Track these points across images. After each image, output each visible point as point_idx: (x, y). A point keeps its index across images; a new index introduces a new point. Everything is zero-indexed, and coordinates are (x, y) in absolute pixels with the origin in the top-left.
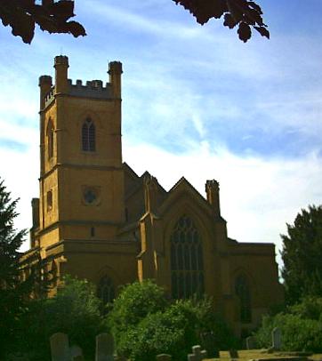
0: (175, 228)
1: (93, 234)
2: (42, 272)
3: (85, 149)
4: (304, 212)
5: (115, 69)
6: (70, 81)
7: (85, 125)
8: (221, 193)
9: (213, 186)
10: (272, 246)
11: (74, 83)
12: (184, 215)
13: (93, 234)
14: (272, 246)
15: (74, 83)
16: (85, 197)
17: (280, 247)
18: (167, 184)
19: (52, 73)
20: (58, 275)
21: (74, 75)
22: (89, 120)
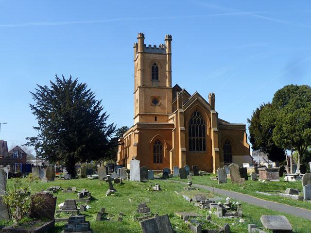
0: (192, 116)
1: (156, 120)
2: (49, 120)
3: (153, 78)
4: (258, 109)
5: (169, 39)
6: (145, 45)
7: (153, 67)
8: (216, 99)
9: (213, 97)
10: (244, 126)
11: (147, 46)
12: (197, 110)
13: (156, 120)
14: (244, 126)
15: (147, 46)
16: (153, 102)
17: (248, 125)
18: (192, 93)
19: (139, 41)
20: (143, 220)
21: (147, 42)
22: (155, 64)
